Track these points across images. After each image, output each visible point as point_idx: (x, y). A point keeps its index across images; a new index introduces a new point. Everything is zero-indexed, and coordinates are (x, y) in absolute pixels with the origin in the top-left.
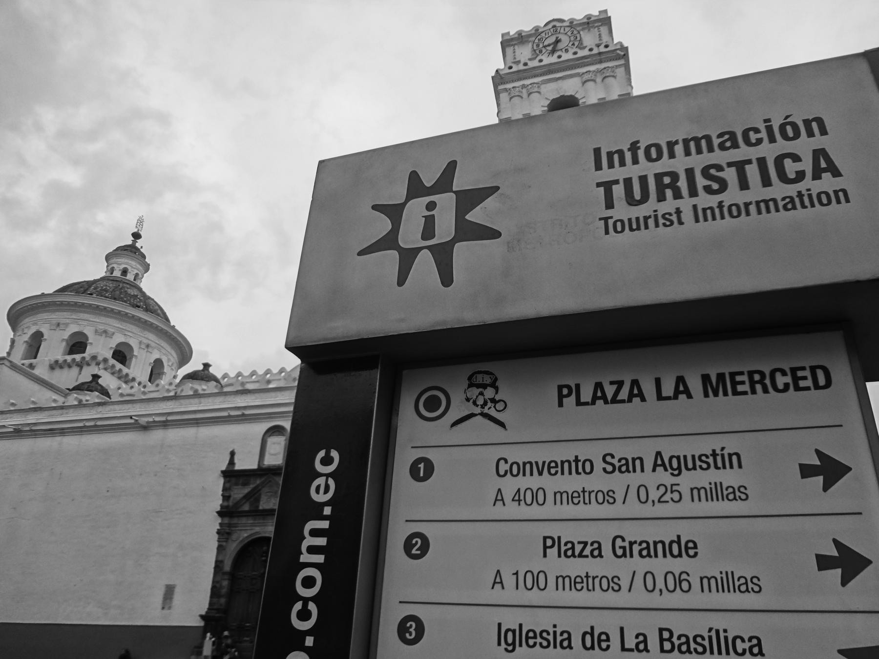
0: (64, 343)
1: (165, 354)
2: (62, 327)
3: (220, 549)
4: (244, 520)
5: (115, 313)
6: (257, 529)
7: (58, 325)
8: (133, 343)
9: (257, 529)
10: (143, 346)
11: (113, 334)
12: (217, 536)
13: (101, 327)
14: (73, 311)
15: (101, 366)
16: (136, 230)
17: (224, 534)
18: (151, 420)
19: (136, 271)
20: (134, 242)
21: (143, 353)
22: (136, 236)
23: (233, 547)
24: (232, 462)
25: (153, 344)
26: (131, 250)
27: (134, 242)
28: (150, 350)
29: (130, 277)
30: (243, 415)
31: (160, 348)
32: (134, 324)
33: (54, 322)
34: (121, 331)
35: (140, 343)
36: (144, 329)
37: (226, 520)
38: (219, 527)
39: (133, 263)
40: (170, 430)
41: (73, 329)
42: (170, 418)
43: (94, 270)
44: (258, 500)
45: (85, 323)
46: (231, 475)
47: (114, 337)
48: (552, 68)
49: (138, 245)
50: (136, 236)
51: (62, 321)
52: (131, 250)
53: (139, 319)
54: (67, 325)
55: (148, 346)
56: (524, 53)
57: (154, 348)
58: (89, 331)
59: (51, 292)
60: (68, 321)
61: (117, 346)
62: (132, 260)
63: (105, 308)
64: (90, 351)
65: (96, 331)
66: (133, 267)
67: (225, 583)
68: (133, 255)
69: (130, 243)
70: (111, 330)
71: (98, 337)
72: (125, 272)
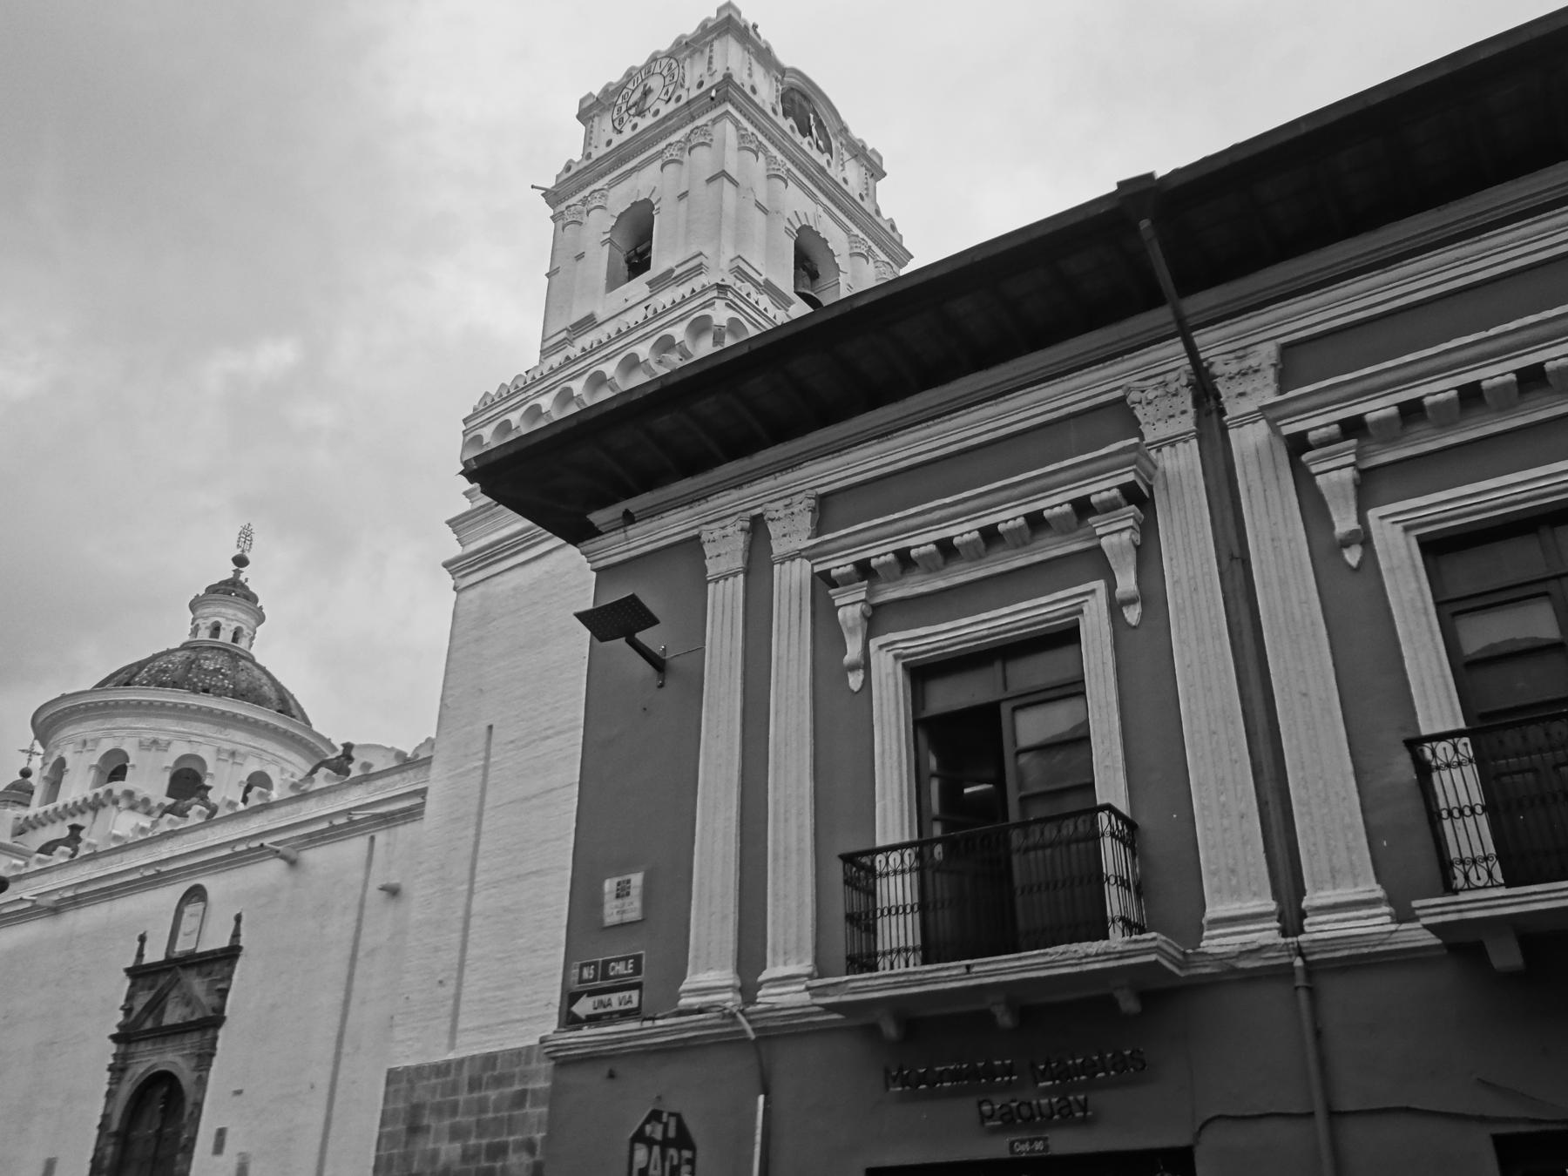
0: (93, 772)
1: (270, 763)
2: (89, 745)
3: (110, 1095)
4: (142, 1047)
5: (170, 709)
6: (155, 1059)
7: (85, 743)
8: (206, 753)
9: (155, 1059)
10: (224, 756)
11: (169, 743)
12: (108, 1075)
13: (150, 736)
14: (139, 715)
15: (123, 804)
16: (238, 552)
17: (118, 1070)
18: (56, 897)
19: (235, 625)
20: (237, 573)
21: (227, 768)
22: (240, 561)
23: (126, 1090)
24: (140, 955)
25: (242, 749)
26: (233, 590)
27: (237, 573)
28: (238, 760)
29: (225, 637)
30: (159, 873)
31: (259, 754)
32: (204, 722)
33: (79, 740)
34: (182, 736)
35: (219, 751)
36: (226, 726)
37: (123, 1047)
38: (111, 1061)
39: (230, 612)
40: (83, 911)
41: (107, 745)
42: (80, 891)
43: (173, 631)
44: (162, 1012)
45: (123, 733)
46: (139, 973)
47: (172, 748)
48: (623, 152)
49: (242, 578)
50: (240, 561)
51: (90, 736)
52: (233, 590)
53: (211, 712)
54: (96, 741)
55: (233, 754)
56: (605, 125)
57: (245, 756)
58: (129, 747)
59: (89, 688)
60: (99, 734)
61: (178, 762)
62: (225, 606)
63: (151, 703)
64: (129, 783)
65: (141, 744)
66: (230, 617)
67: (110, 1150)
68: (226, 597)
69: (230, 575)
70: (163, 737)
71: (145, 753)
72: (216, 629)
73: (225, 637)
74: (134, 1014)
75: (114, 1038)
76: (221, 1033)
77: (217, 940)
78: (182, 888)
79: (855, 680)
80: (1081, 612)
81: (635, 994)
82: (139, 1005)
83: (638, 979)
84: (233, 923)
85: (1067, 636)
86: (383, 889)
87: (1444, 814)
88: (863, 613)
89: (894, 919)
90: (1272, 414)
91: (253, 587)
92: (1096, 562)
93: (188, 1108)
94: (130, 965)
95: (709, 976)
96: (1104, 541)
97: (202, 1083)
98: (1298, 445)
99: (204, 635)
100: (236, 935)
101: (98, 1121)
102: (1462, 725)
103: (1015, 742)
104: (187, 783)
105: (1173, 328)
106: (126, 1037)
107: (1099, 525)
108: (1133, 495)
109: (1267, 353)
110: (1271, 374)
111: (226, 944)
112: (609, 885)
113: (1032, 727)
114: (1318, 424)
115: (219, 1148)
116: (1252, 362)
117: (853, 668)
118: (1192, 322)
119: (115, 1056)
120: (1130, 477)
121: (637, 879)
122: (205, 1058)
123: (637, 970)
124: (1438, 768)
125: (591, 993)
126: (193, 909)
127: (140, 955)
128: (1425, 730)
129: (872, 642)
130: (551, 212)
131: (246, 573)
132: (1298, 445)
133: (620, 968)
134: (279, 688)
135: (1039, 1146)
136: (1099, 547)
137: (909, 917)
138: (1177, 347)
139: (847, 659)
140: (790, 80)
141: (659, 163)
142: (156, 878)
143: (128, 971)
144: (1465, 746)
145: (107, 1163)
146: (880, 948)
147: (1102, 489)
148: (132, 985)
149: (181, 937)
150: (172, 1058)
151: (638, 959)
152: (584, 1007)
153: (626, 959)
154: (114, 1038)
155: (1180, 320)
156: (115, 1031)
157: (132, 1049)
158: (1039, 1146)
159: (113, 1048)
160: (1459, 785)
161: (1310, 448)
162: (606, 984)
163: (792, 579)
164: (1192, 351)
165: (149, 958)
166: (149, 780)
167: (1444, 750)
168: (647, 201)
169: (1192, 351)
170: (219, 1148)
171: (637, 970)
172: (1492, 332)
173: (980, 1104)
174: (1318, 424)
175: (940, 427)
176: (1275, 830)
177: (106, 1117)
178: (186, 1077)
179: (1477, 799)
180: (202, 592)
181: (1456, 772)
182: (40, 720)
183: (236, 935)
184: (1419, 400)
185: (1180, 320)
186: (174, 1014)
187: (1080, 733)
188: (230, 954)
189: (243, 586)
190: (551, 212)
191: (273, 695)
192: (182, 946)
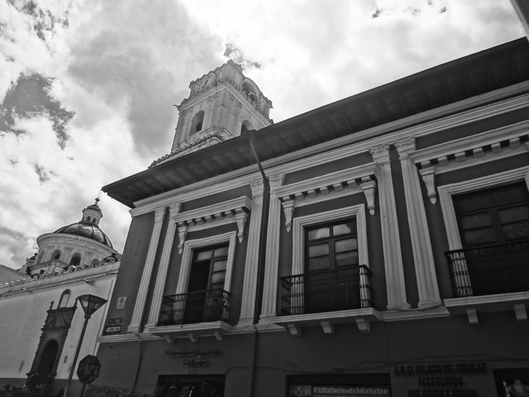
20: (96, 203)
24: (51, 307)
27: (96, 203)
75: (42, 329)
76: (70, 330)
77: (70, 305)
78: (61, 290)
79: (288, 230)
80: (357, 212)
81: (119, 327)
82: (50, 320)
83: (120, 324)
84: (50, 305)
85: (225, 245)
87: (455, 274)
88: (292, 211)
89: (299, 298)
90: (411, 157)
91: (100, 207)
92: (361, 198)
94: (48, 309)
95: (135, 324)
96: (365, 192)
98: (419, 166)
101: (36, 351)
102: (461, 248)
103: (212, 270)
104: (76, 260)
105: (259, 169)
106: (45, 329)
107: (364, 186)
108: (373, 178)
109: (281, 176)
110: (281, 181)
111: (73, 306)
112: (119, 299)
113: (217, 266)
114: (425, 161)
115: (65, 361)
116: (278, 178)
117: (432, 196)
118: (263, 168)
119: (42, 334)
120: (244, 205)
121: (125, 298)
123: (121, 322)
124: (454, 260)
125: (110, 327)
126: (66, 296)
127: (51, 307)
128: (451, 249)
129: (294, 219)
130: (179, 112)
131: (99, 203)
132: (419, 166)
133: (117, 321)
135: (195, 372)
136: (363, 193)
137: (301, 297)
138: (260, 173)
139: (286, 223)
140: (246, 80)
141: (207, 101)
143: (48, 311)
144: (462, 255)
145: (37, 363)
146: (291, 306)
147: (365, 176)
148: (48, 316)
151: (122, 319)
152: (108, 330)
153: (119, 318)
154: (42, 329)
155: (260, 166)
156: (42, 327)
158: (195, 372)
159: (41, 332)
160: (460, 265)
161: (284, 201)
162: (114, 324)
163: (172, 224)
164: (263, 174)
165: (53, 309)
166: (66, 257)
167: (457, 255)
168: (203, 111)
169: (263, 174)
170: (65, 361)
171: (121, 322)
172: (323, 176)
173: (184, 361)
174: (425, 161)
175: (203, 190)
176: (427, 274)
177: (38, 350)
180: (86, 208)
181: (459, 262)
184: (472, 150)
185: (260, 166)
186: (58, 324)
187: (224, 269)
189: (97, 207)
190: (179, 112)
191: (101, 237)
192: (62, 306)
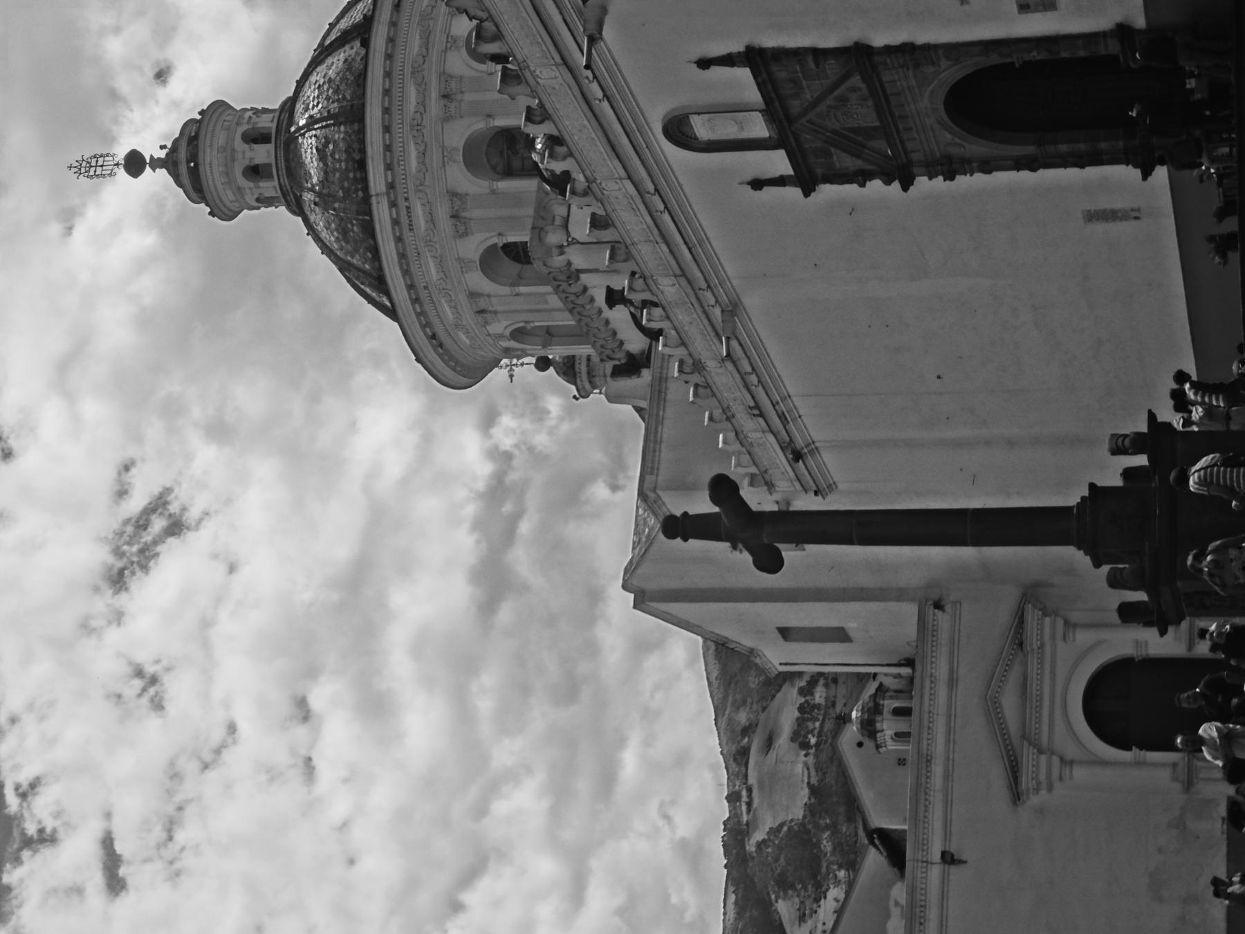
16: (121, 172)
17: (949, 168)
20: (156, 164)
22: (135, 164)
27: (156, 164)
50: (135, 164)
54: (473, 295)
69: (162, 173)
72: (255, 172)
73: (263, 154)
74: (868, 167)
75: (906, 185)
82: (847, 162)
86: (961, 862)
93: (995, 59)
97: (954, 50)
99: (269, 187)
100: (728, 60)
122: (911, 54)
126: (702, 128)
131: (151, 149)
134: (323, 53)
142: (658, 195)
149: (746, 135)
150: (925, 104)
154: (906, 185)
156: (896, 185)
157: (915, 157)
178: (950, 74)
179: (791, 509)
182: (465, 381)
183: (728, 60)
188: (754, 58)
192: (759, 128)
